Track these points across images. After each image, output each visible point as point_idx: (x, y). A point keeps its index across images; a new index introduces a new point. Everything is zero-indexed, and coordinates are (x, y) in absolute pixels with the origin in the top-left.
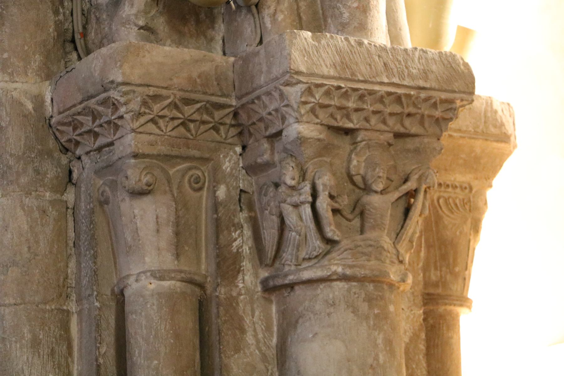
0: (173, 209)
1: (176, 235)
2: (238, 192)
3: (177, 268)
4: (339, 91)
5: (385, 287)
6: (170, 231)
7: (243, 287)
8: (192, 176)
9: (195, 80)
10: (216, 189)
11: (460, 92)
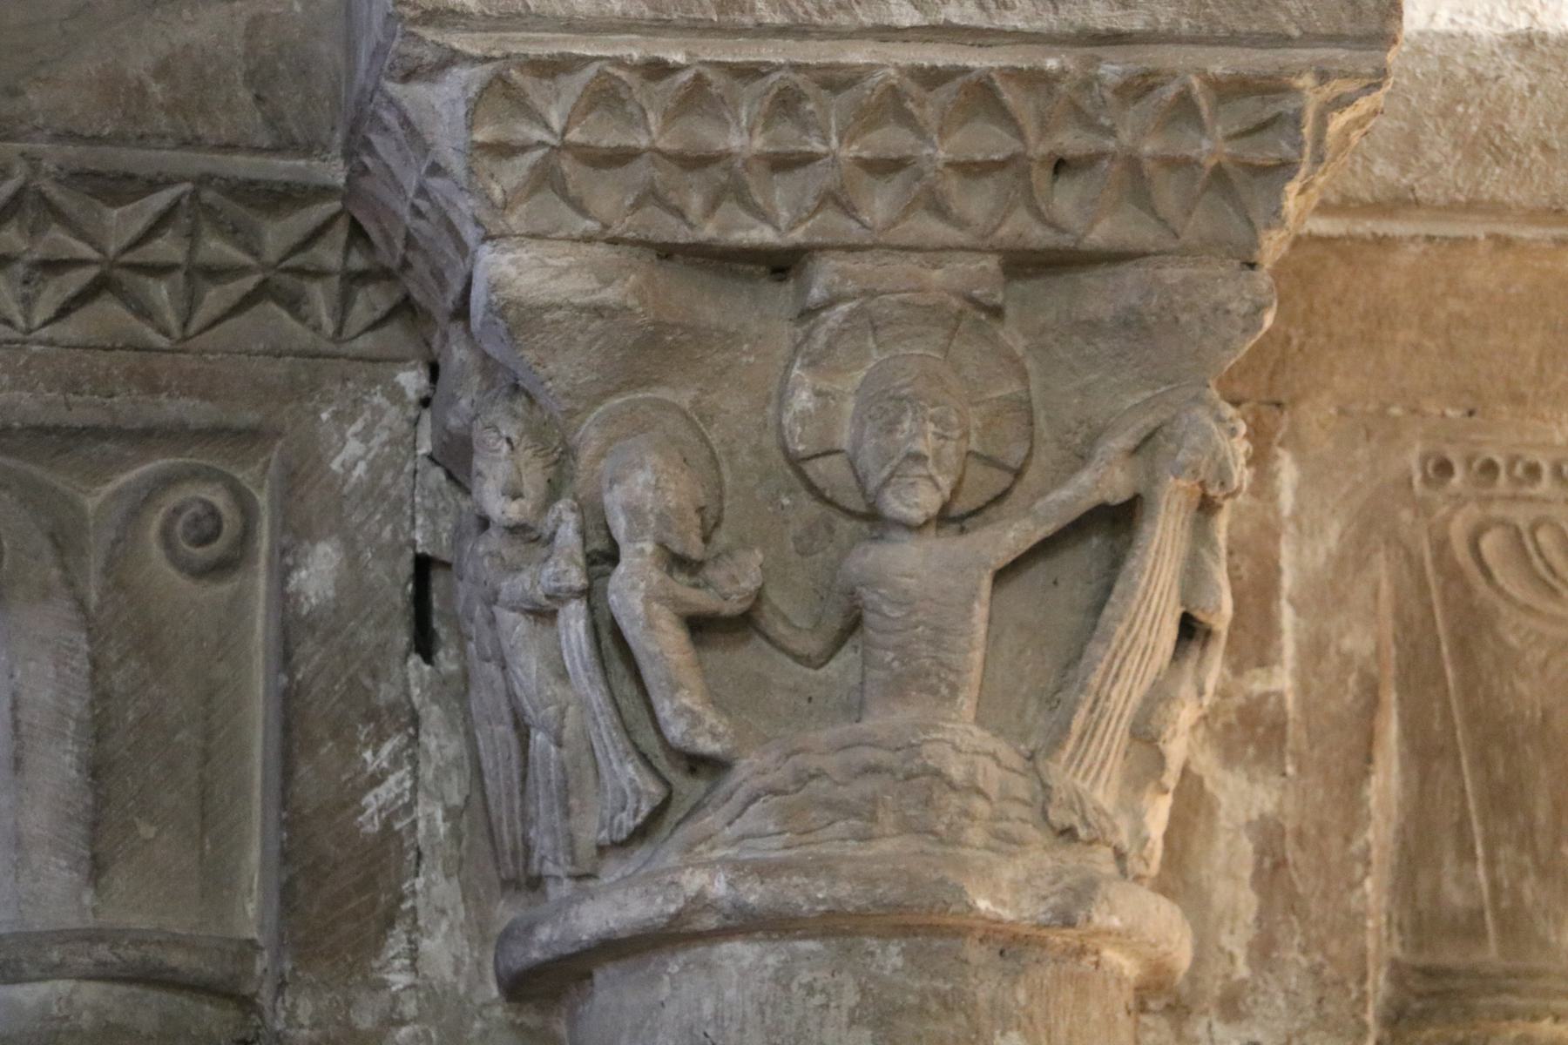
0: (81, 663)
1: (93, 775)
2: (406, 567)
3: (91, 922)
4: (665, 83)
5: (975, 952)
6: (68, 758)
7: (412, 986)
8: (177, 512)
9: (141, 90)
10: (289, 560)
11: (1311, 39)
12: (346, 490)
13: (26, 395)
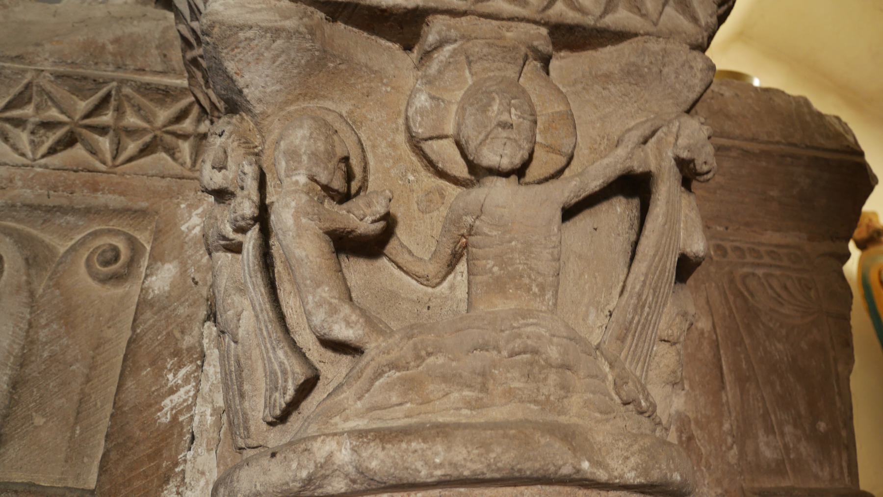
0: (24, 325)
1: (14, 388)
9: (103, 47)
12: (187, 239)
13: (29, 191)
